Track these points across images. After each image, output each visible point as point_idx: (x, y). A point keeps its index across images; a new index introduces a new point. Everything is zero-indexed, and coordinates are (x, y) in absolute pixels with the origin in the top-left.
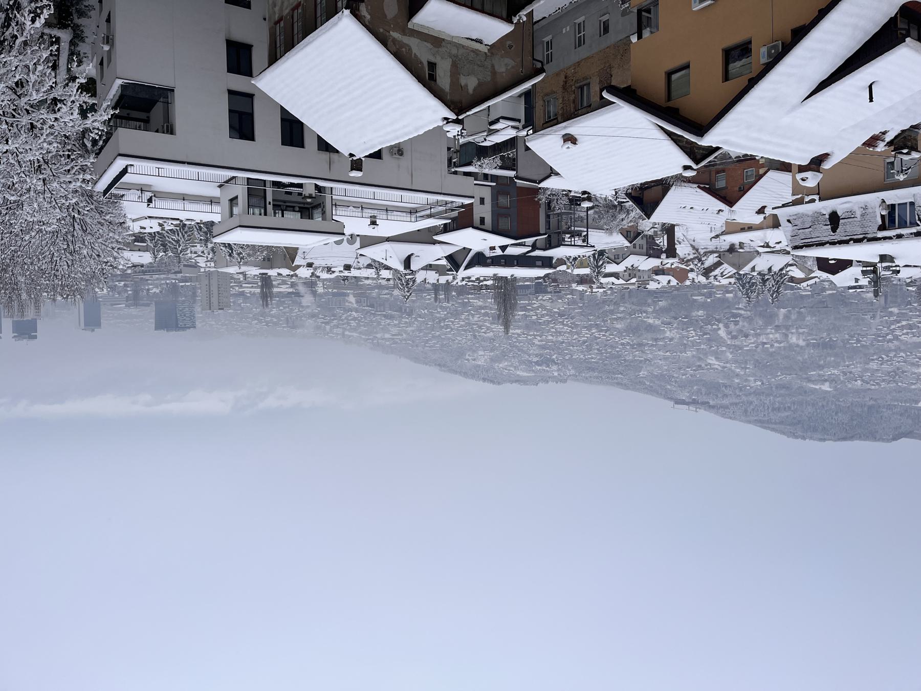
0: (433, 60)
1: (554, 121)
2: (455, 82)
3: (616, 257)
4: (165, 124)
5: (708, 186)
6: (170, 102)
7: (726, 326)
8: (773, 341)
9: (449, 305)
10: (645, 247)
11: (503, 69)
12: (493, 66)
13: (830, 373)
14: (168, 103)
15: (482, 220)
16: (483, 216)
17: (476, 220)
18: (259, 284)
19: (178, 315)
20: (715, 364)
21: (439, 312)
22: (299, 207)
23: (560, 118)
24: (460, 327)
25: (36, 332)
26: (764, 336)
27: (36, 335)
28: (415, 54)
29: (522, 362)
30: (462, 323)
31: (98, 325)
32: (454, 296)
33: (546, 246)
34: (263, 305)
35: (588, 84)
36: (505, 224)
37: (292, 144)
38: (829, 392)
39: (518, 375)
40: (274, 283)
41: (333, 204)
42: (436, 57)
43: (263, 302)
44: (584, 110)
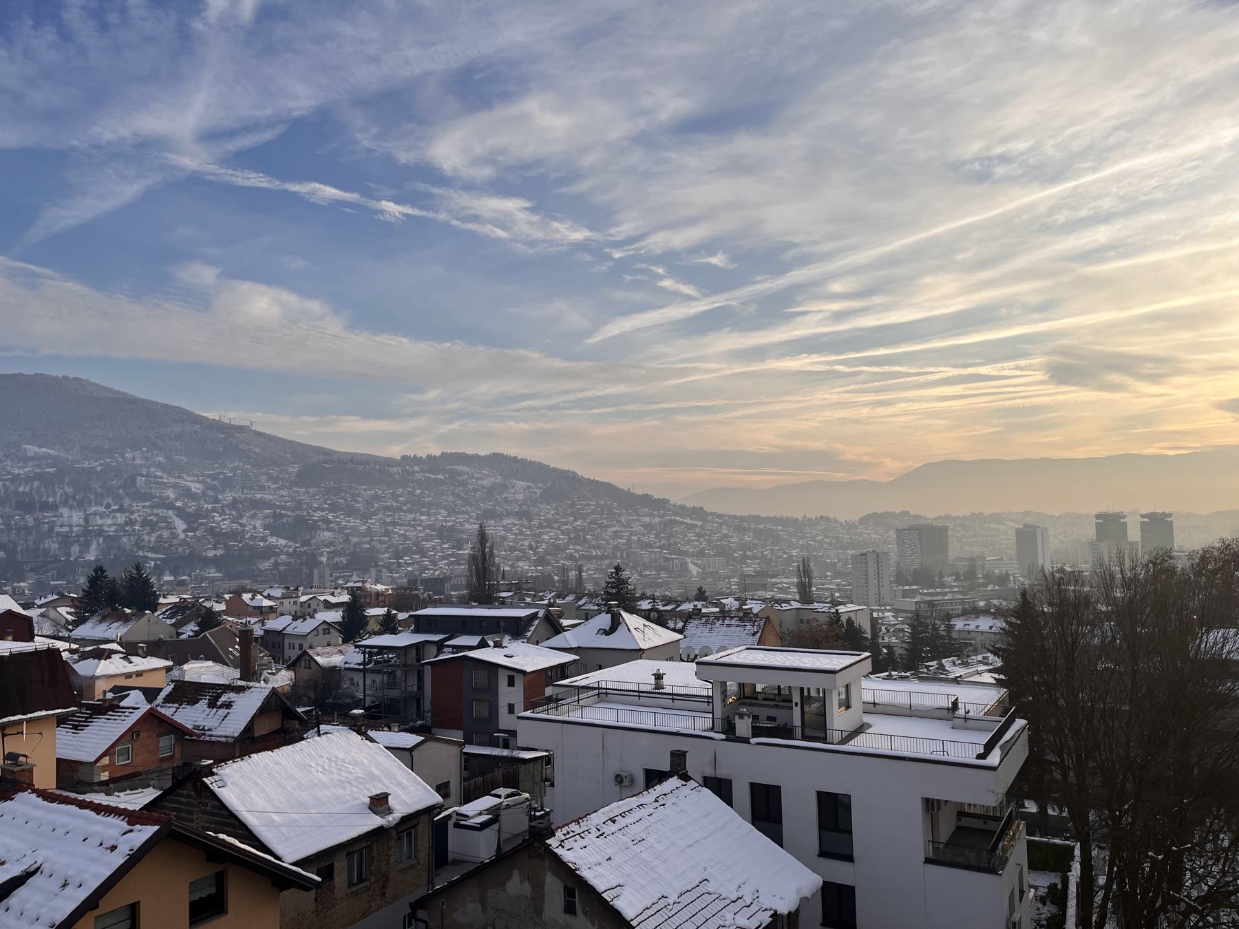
0: (569, 918)
1: (401, 829)
2: (538, 887)
3: (327, 632)
4: (935, 812)
5: (187, 737)
6: (931, 844)
7: (174, 535)
8: (107, 516)
9: (563, 562)
10: (286, 645)
11: (470, 906)
12: (484, 910)
13: (26, 470)
14: (933, 842)
15: (511, 683)
16: (511, 688)
17: (519, 682)
18: (814, 589)
19: (918, 546)
20: (192, 481)
21: (577, 551)
22: (757, 699)
23: (393, 835)
24: (548, 532)
25: (1096, 523)
26: (119, 522)
27: (1097, 519)
28: (594, 925)
29: (464, 484)
30: (546, 537)
31: (1019, 533)
32: (556, 575)
33: (423, 647)
34: (808, 561)
35: (350, 884)
36: (479, 678)
37: (767, 788)
38: (27, 443)
39: (468, 466)
40: (796, 590)
41: (711, 704)
42: (565, 922)
43: (809, 565)
44: (357, 847)
